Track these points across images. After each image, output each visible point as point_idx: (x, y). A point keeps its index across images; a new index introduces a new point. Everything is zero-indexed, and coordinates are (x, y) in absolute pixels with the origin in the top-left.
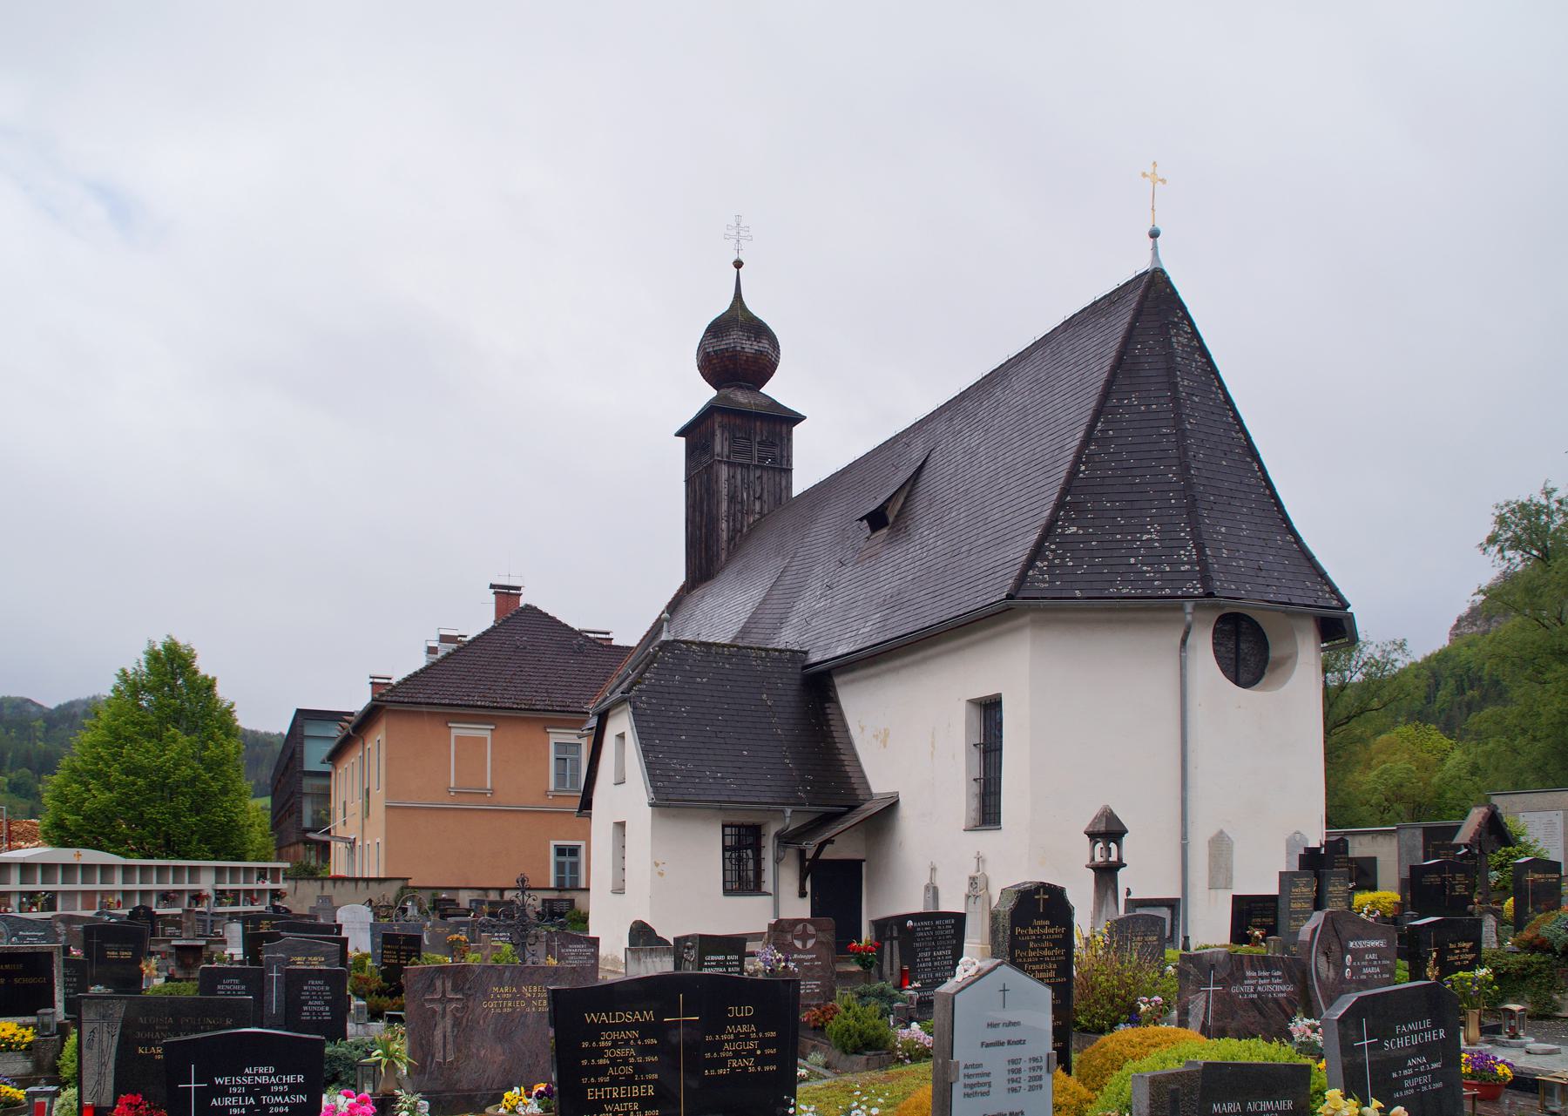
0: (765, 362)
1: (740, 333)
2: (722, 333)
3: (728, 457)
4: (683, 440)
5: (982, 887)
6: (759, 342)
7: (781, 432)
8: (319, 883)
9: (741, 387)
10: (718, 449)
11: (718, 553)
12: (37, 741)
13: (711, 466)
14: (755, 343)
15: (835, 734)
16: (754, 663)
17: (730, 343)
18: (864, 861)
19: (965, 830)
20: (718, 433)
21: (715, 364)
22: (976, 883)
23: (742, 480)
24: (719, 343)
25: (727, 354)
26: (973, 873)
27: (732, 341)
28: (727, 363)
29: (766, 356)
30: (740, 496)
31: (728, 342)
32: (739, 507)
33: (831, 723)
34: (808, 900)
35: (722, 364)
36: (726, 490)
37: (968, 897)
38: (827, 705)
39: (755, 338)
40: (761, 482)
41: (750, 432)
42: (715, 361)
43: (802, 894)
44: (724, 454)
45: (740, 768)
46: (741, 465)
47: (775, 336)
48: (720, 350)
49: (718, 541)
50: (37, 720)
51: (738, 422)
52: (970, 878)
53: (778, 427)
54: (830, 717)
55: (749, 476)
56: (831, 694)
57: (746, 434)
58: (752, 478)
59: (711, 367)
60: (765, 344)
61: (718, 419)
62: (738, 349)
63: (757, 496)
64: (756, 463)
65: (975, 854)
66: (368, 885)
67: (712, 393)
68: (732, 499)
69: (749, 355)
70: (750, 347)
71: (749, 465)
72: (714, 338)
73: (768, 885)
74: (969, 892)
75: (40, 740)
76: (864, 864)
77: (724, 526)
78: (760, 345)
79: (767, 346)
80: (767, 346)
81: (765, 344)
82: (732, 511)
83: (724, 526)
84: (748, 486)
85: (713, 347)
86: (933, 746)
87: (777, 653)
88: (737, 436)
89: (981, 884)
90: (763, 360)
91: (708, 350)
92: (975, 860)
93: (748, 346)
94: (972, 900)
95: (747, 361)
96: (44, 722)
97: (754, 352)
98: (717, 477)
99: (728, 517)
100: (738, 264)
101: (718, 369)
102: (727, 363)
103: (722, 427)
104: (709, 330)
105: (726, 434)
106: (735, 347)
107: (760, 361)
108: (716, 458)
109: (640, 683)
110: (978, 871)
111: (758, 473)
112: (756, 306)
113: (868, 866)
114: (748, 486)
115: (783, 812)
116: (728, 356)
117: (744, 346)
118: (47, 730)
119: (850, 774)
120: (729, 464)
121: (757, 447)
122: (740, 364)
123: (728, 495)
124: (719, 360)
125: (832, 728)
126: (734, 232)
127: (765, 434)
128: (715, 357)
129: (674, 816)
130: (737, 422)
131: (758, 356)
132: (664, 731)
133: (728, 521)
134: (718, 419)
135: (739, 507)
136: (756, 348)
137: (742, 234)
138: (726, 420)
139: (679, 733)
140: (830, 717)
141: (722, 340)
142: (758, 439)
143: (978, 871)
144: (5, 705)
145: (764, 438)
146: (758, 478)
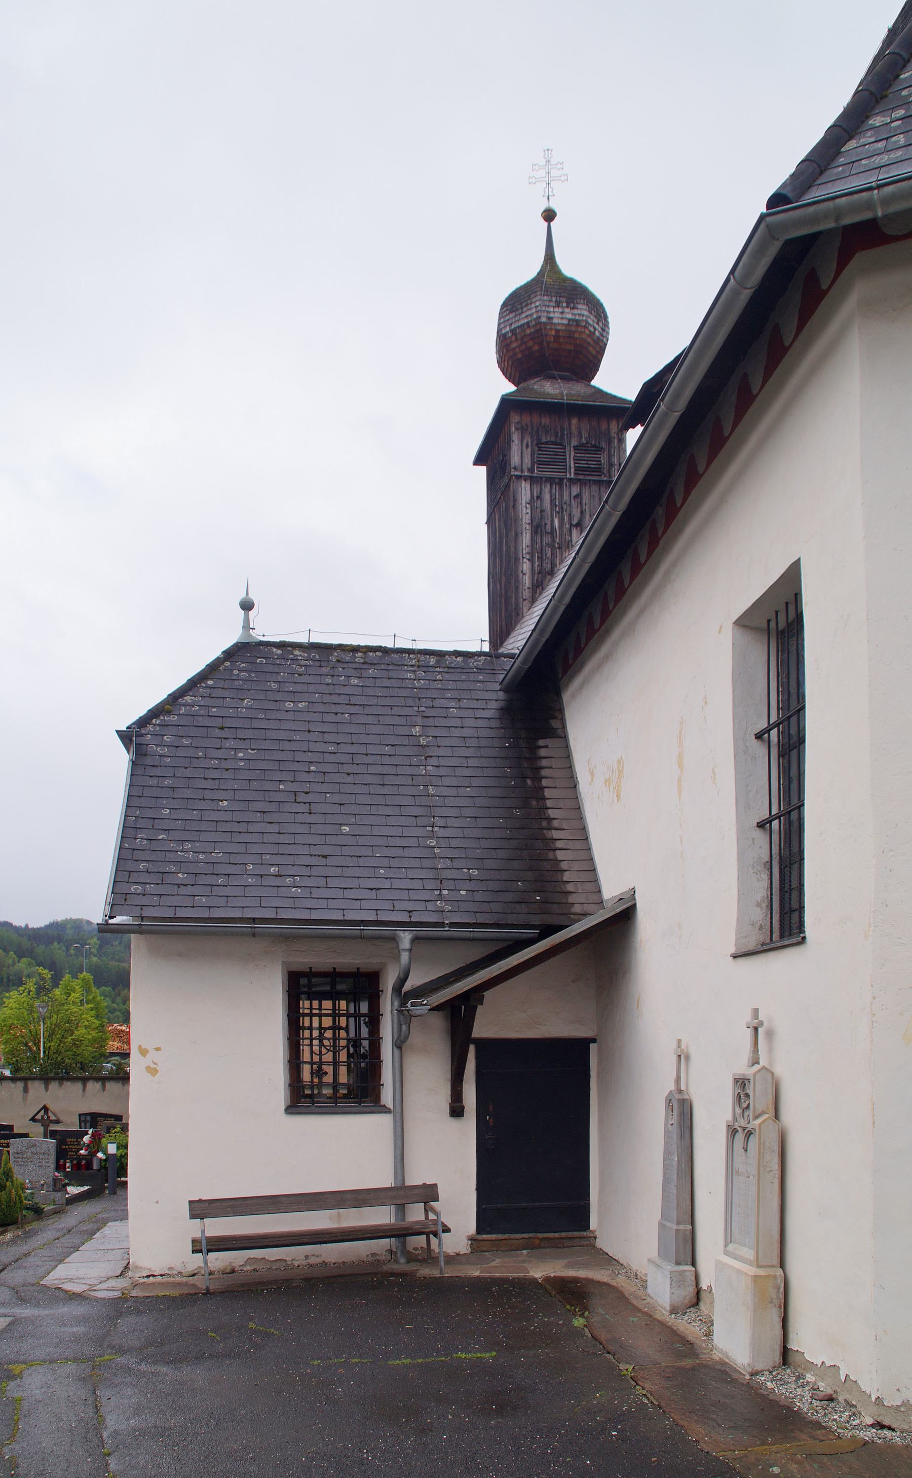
0: (584, 336)
1: (545, 298)
2: (521, 304)
3: (531, 470)
4: (483, 469)
5: (759, 1109)
6: (574, 308)
7: (609, 429)
8: (20, 1085)
9: (553, 378)
10: (515, 459)
11: (517, 605)
12: (93, 956)
13: (508, 486)
14: (567, 310)
15: (547, 793)
16: (409, 675)
17: (531, 315)
18: (594, 1040)
19: (735, 957)
20: (516, 438)
21: (514, 349)
22: (747, 1096)
23: (552, 501)
24: (517, 318)
25: (528, 332)
26: (742, 1068)
27: (534, 310)
28: (530, 343)
29: (585, 327)
30: (549, 523)
31: (528, 313)
32: (547, 539)
33: (544, 773)
34: (469, 1126)
35: (524, 347)
36: (528, 516)
37: (732, 1132)
38: (541, 742)
39: (568, 304)
40: (581, 503)
41: (563, 434)
42: (514, 345)
43: (457, 1111)
44: (525, 467)
45: (325, 857)
46: (551, 480)
47: (601, 306)
48: (519, 327)
49: (517, 588)
50: (92, 938)
51: (545, 421)
52: (736, 1081)
53: (604, 426)
54: (544, 763)
55: (561, 496)
56: (555, 724)
57: (556, 436)
58: (566, 497)
59: (511, 353)
60: (582, 311)
61: (515, 418)
62: (543, 320)
63: (574, 522)
64: (572, 476)
65: (748, 1017)
66: (26, 1090)
67: (511, 388)
68: (537, 528)
69: (559, 328)
70: (560, 316)
71: (561, 480)
72: (512, 312)
73: (387, 1096)
74: (735, 1119)
75: (95, 956)
76: (593, 1047)
77: (526, 566)
78: (575, 312)
79: (586, 313)
80: (586, 313)
81: (582, 311)
82: (538, 546)
83: (526, 566)
84: (560, 508)
85: (511, 325)
86: (681, 766)
87: (459, 659)
88: (544, 440)
89: (760, 1099)
90: (581, 333)
91: (503, 332)
92: (749, 1033)
93: (557, 315)
94: (740, 1137)
95: (557, 337)
96: (98, 940)
97: (566, 322)
98: (515, 501)
99: (532, 554)
100: (549, 216)
101: (520, 356)
102: (530, 343)
103: (523, 430)
104: (504, 305)
105: (528, 439)
106: (539, 317)
107: (577, 335)
108: (513, 473)
109: (169, 712)
110: (756, 1062)
111: (575, 490)
112: (568, 267)
113: (600, 1051)
114: (560, 508)
115: (394, 939)
116: (531, 334)
117: (551, 315)
118: (101, 947)
119: (564, 866)
120: (532, 480)
121: (573, 453)
122: (548, 343)
123: (531, 524)
124: (519, 343)
125: (544, 783)
126: (542, 173)
127: (585, 434)
128: (513, 338)
129: (180, 955)
130: (543, 421)
131: (573, 329)
132: (188, 793)
133: (531, 560)
134: (515, 418)
135: (547, 539)
136: (570, 316)
137: (554, 173)
138: (526, 419)
139: (217, 795)
140: (544, 763)
141: (522, 313)
142: (574, 442)
143: (756, 1062)
144: (68, 926)
145: (584, 441)
146: (576, 497)
